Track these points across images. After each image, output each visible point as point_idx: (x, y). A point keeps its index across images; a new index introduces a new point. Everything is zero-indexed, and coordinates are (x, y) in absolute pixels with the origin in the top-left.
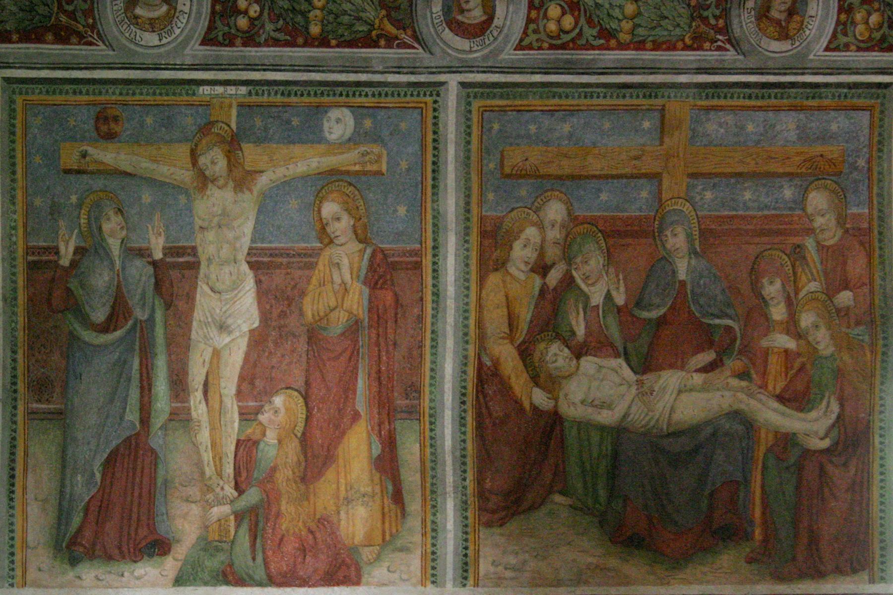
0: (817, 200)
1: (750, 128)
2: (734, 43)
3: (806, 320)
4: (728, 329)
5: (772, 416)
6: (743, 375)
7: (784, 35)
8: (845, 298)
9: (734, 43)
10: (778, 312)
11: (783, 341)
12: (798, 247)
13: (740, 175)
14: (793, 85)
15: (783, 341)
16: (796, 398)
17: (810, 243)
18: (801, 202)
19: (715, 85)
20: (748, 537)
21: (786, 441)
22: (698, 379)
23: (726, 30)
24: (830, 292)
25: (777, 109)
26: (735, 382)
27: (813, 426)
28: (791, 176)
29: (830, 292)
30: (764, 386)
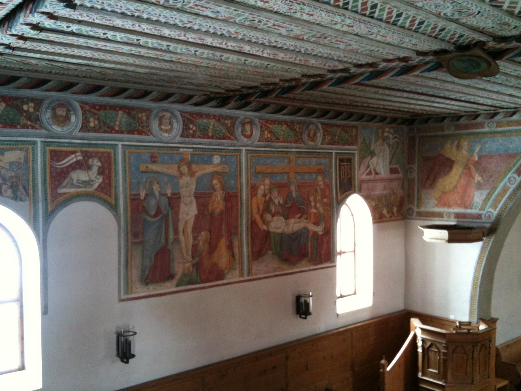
0: (320, 178)
1: (307, 162)
2: (303, 142)
3: (318, 205)
4: (303, 208)
5: (312, 228)
6: (306, 219)
7: (313, 141)
8: (325, 200)
9: (303, 142)
10: (313, 204)
11: (314, 210)
12: (316, 189)
13: (305, 173)
14: (315, 152)
15: (314, 210)
16: (316, 224)
17: (318, 188)
18: (316, 179)
19: (300, 152)
20: (308, 256)
21: (315, 233)
22: (298, 220)
23: (301, 139)
24: (322, 199)
25: (312, 157)
26: (305, 220)
27: (319, 230)
28: (315, 173)
29: (322, 199)
30: (310, 221)
